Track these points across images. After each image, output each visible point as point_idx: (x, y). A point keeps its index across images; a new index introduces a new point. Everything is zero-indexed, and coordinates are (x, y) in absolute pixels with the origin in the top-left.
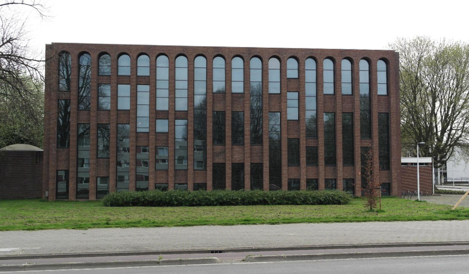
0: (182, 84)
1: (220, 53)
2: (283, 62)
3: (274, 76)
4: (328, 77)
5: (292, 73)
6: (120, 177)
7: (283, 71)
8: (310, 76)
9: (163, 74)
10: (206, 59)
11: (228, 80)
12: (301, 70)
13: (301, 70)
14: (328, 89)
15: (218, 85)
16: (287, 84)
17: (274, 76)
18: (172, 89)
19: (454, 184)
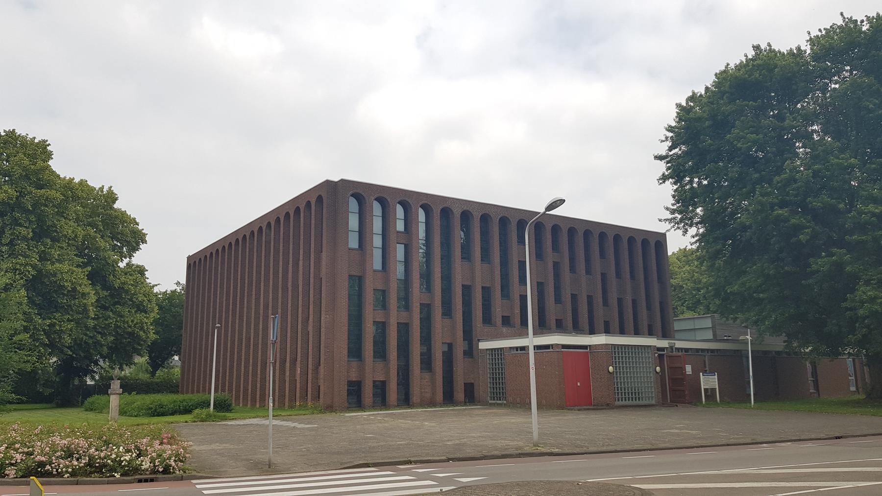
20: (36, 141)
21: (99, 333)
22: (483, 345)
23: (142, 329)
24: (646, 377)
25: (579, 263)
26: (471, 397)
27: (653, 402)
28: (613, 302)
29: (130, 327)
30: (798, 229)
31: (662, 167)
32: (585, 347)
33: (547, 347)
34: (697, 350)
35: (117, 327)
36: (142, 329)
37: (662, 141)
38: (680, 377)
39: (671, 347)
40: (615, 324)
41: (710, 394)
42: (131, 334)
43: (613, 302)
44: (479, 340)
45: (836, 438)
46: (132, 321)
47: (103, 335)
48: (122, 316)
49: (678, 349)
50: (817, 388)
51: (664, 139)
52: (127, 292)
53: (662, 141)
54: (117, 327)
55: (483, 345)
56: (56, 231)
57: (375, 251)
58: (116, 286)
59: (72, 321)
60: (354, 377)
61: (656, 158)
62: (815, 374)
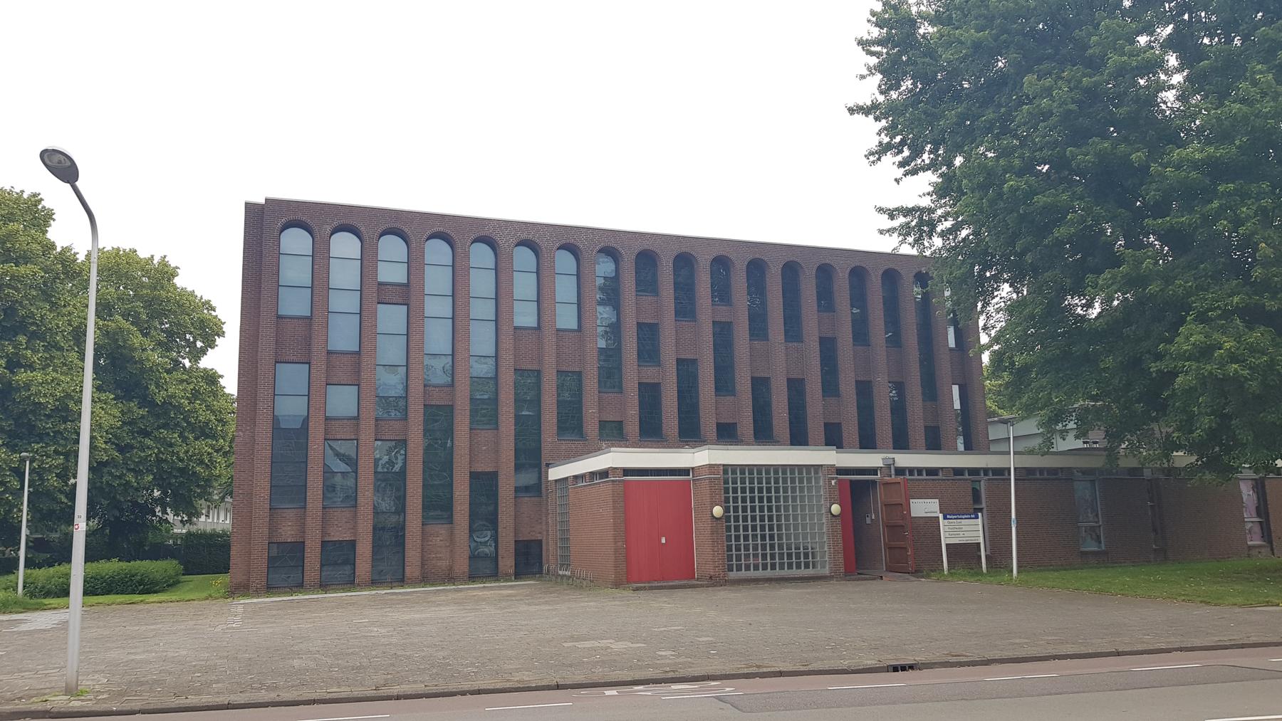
0: (482, 309)
1: (300, 216)
2: (414, 245)
3: (345, 275)
4: (524, 286)
5: (391, 273)
6: (273, 563)
7: (368, 260)
8: (437, 280)
9: (437, 280)
10: (452, 247)
11: (542, 299)
12: (414, 263)
13: (414, 263)
14: (525, 316)
15: (525, 316)
16: (376, 293)
17: (345, 275)
18: (459, 321)
19: (967, 476)
20: (25, 196)
21: (129, 470)
22: (555, 473)
23: (201, 462)
24: (819, 520)
25: (693, 319)
26: (529, 561)
27: (826, 571)
28: (848, 388)
29: (181, 460)
30: (1056, 214)
31: (870, 131)
32: (685, 472)
33: (604, 474)
34: (958, 471)
35: (159, 461)
36: (201, 462)
37: (863, 77)
38: (900, 522)
39: (889, 467)
40: (851, 430)
41: (964, 555)
42: (183, 471)
43: (848, 388)
44: (548, 465)
45: (895, 669)
46: (187, 452)
47: (137, 472)
48: (171, 445)
49: (900, 471)
50: (1267, 533)
51: (865, 72)
52: (178, 408)
53: (863, 77)
54: (159, 461)
55: (555, 473)
56: (33, 324)
57: (474, 327)
58: (159, 400)
59: (62, 454)
60: (288, 532)
61: (852, 111)
62: (1262, 510)
